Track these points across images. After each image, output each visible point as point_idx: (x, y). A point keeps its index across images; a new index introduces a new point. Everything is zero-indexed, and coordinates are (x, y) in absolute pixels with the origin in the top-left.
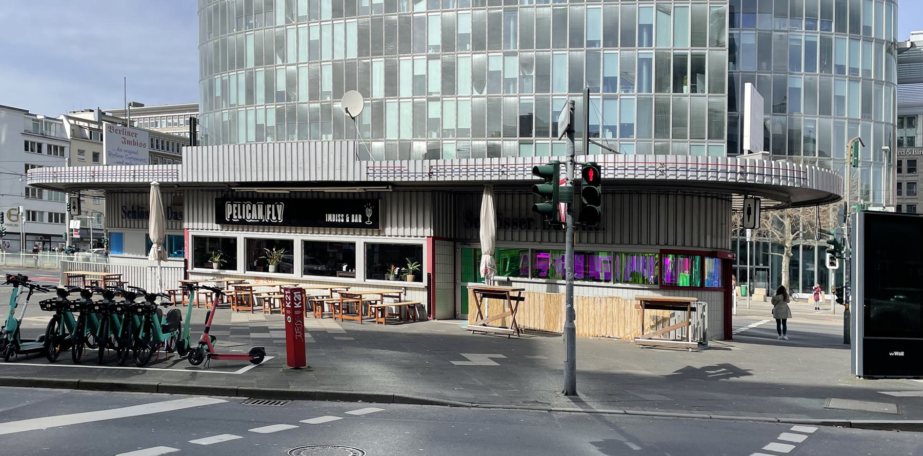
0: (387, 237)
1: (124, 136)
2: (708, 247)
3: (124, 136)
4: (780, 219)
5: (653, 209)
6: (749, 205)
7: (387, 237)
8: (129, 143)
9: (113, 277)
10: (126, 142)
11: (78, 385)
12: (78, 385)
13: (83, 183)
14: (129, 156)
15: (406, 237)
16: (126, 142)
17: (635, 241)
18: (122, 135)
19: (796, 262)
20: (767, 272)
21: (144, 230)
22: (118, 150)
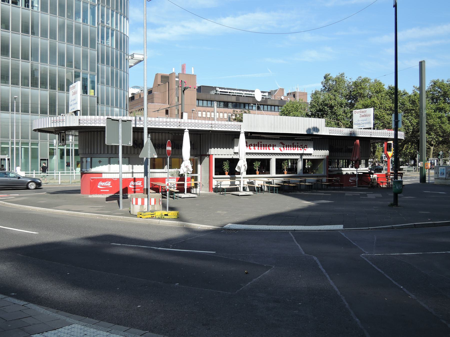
0: (312, 156)
1: (361, 114)
2: (92, 153)
3: (361, 114)
4: (425, 129)
5: (99, 138)
6: (63, 135)
7: (312, 156)
8: (363, 116)
9: (366, 183)
10: (362, 116)
11: (118, 198)
12: (118, 198)
13: (79, 143)
14: (363, 122)
15: (226, 155)
16: (362, 116)
17: (106, 152)
18: (360, 114)
19: (37, 156)
20: (47, 161)
21: (87, 155)
22: (358, 121)
